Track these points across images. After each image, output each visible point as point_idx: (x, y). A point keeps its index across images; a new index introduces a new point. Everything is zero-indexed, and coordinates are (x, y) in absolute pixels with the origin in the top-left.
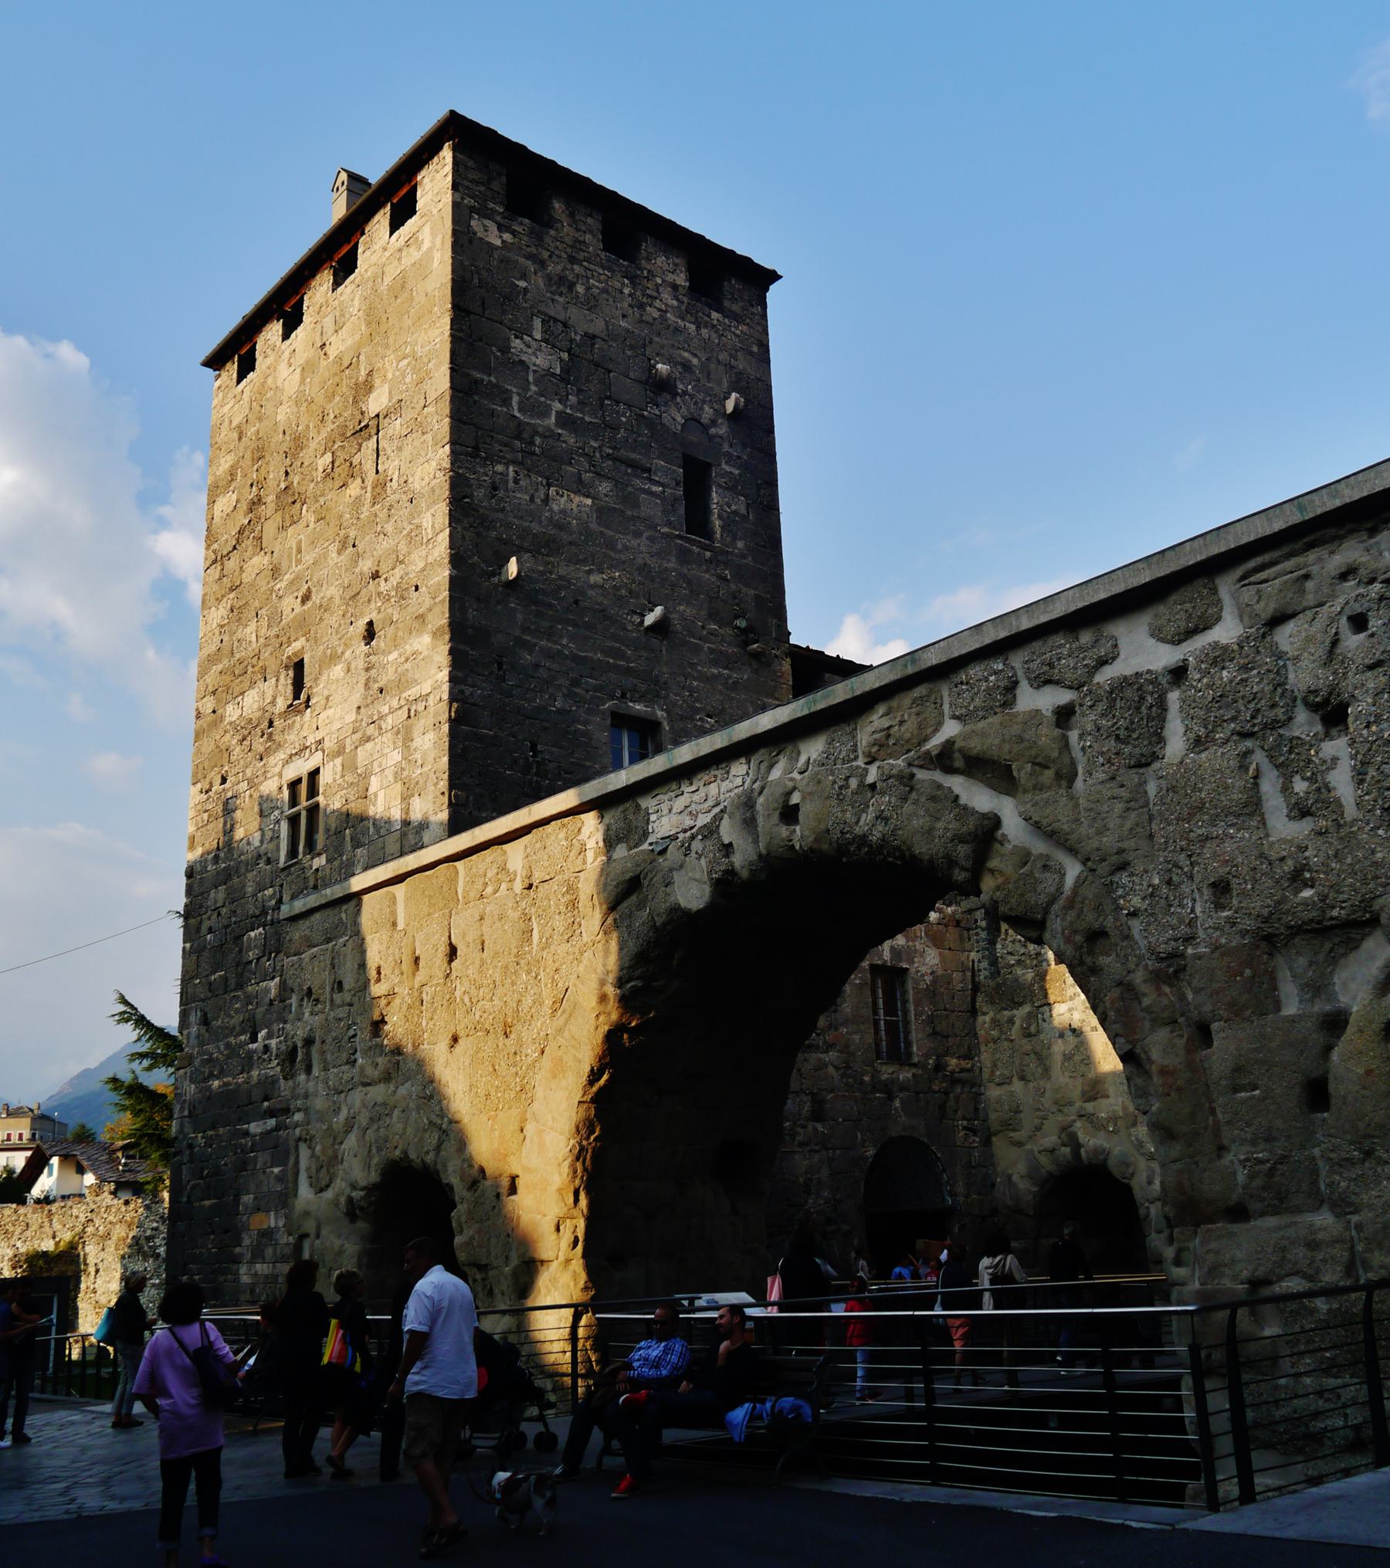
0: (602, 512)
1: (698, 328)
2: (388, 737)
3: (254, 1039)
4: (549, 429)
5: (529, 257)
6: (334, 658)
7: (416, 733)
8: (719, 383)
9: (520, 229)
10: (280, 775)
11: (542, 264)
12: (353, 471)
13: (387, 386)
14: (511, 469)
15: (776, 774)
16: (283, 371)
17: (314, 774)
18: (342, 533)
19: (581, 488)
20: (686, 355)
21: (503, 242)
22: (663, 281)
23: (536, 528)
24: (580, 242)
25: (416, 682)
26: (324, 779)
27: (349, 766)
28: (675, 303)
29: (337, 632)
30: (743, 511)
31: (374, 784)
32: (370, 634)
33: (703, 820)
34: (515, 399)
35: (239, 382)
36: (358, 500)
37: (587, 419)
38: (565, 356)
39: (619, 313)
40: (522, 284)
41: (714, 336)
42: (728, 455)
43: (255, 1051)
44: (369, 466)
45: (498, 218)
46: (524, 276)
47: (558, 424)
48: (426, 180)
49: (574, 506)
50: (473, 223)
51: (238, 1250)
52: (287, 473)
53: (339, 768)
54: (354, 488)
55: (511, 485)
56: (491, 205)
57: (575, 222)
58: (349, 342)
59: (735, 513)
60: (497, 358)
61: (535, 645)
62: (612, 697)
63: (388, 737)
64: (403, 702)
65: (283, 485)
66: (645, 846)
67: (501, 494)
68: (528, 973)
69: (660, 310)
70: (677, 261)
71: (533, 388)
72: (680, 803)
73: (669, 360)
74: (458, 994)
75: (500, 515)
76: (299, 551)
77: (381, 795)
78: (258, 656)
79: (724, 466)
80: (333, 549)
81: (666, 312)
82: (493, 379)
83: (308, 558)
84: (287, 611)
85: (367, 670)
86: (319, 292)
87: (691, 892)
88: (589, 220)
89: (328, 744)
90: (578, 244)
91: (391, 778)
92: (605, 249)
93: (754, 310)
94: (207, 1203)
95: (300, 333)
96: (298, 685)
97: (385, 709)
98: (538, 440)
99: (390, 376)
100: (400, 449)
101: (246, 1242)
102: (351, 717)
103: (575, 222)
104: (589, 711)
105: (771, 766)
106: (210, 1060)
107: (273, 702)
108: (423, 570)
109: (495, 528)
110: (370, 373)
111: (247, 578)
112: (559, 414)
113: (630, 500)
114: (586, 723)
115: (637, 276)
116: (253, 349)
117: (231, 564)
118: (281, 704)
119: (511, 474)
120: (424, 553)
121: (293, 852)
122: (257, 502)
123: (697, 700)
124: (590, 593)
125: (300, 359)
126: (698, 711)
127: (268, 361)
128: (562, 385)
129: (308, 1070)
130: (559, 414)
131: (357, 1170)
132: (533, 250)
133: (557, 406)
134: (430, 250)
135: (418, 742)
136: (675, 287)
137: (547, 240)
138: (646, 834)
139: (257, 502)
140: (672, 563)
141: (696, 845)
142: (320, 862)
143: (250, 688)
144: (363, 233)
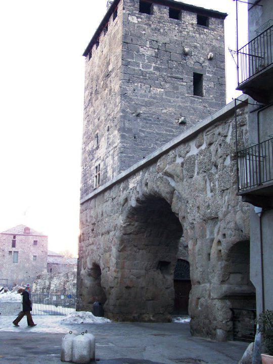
4: (151, 71)
5: (146, 24)
8: (206, 50)
11: (150, 25)
19: (161, 86)
20: (195, 43)
23: (146, 99)
25: (115, 143)
27: (105, 164)
30: (213, 86)
34: (141, 65)
38: (156, 50)
39: (174, 35)
40: (144, 32)
45: (137, 15)
46: (144, 30)
54: (106, 91)
55: (139, 88)
56: (134, 12)
59: (210, 87)
67: (136, 91)
73: (190, 46)
75: (136, 97)
78: (91, 134)
82: (134, 60)
85: (108, 139)
87: (133, 203)
88: (165, 10)
92: (170, 17)
95: (99, 47)
98: (148, 75)
107: (93, 146)
112: (154, 67)
113: (176, 88)
117: (88, 109)
118: (95, 147)
122: (91, 93)
130: (154, 67)
131: (89, 265)
133: (154, 65)
136: (192, 24)
137: (152, 18)
139: (91, 93)
140: (188, 104)
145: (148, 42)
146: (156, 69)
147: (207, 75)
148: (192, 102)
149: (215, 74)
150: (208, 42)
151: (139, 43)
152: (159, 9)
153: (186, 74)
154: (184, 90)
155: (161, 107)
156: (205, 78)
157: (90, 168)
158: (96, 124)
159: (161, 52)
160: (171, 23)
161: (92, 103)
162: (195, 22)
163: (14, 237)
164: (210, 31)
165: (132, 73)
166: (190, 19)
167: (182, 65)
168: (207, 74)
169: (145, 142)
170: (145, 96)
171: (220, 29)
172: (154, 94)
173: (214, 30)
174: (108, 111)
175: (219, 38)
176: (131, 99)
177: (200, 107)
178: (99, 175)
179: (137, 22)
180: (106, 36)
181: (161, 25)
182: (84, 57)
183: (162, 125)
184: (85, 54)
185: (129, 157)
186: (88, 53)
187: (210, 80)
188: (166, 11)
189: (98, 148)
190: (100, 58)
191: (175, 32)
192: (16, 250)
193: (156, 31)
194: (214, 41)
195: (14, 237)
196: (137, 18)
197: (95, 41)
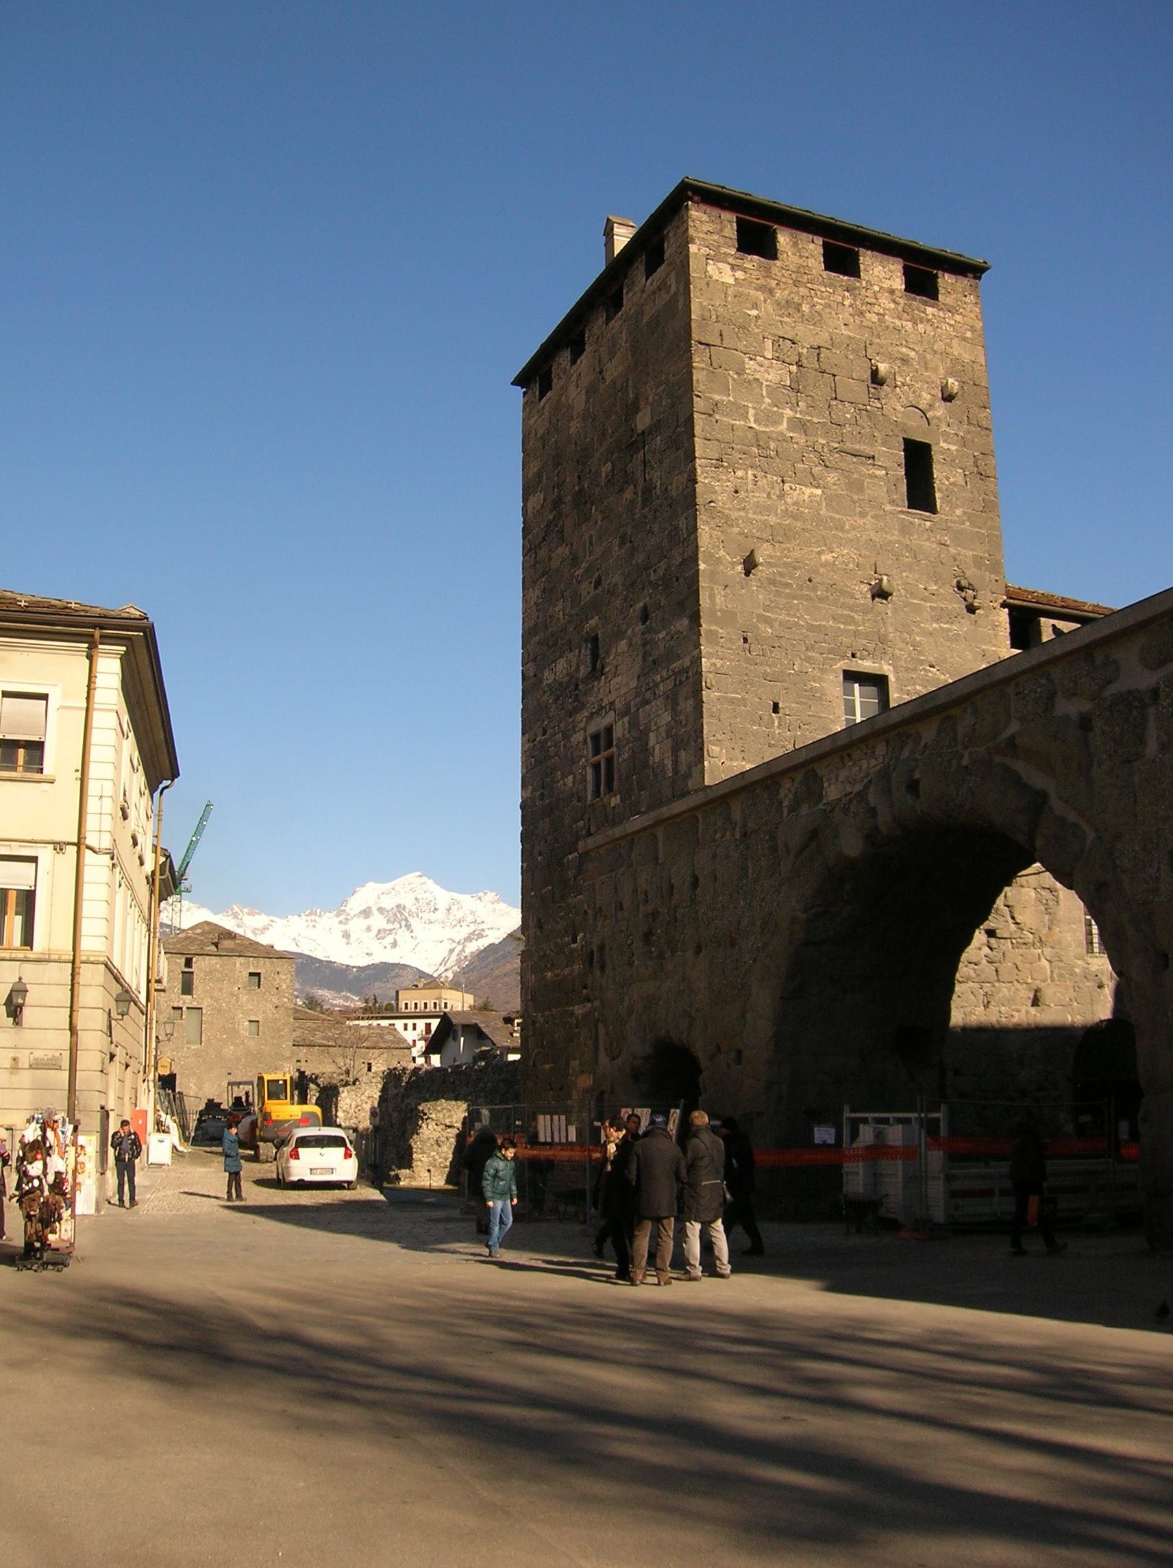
0: (830, 500)
1: (915, 323)
2: (659, 702)
3: (575, 941)
4: (781, 433)
5: (760, 288)
6: (619, 634)
7: (681, 700)
8: (935, 370)
9: (750, 266)
10: (585, 729)
11: (771, 292)
12: (628, 479)
13: (649, 408)
14: (750, 472)
15: (905, 754)
16: (573, 391)
17: (609, 730)
18: (621, 530)
19: (814, 482)
20: (904, 350)
21: (736, 279)
22: (881, 288)
23: (772, 520)
24: (804, 267)
25: (679, 657)
26: (618, 733)
27: (634, 724)
28: (892, 305)
29: (621, 613)
30: (961, 481)
31: (652, 739)
32: (645, 616)
33: (858, 787)
34: (751, 412)
35: (540, 399)
36: (633, 501)
37: (816, 420)
38: (794, 368)
39: (841, 323)
40: (754, 312)
41: (929, 329)
42: (945, 433)
43: (576, 950)
44: (639, 474)
45: (731, 260)
46: (755, 306)
47: (789, 429)
48: (671, 235)
49: (806, 497)
50: (709, 268)
51: (569, 1102)
52: (579, 477)
53: (627, 726)
54: (628, 495)
55: (750, 486)
56: (724, 250)
57: (799, 250)
58: (620, 369)
59: (954, 484)
60: (734, 380)
61: (775, 620)
62: (843, 657)
63: (659, 702)
64: (670, 673)
65: (577, 488)
66: (821, 806)
67: (742, 494)
68: (745, 900)
69: (878, 314)
70: (892, 267)
71: (768, 400)
72: (843, 775)
73: (890, 358)
74: (700, 915)
75: (742, 514)
76: (591, 543)
77: (657, 748)
78: (564, 630)
79: (942, 444)
80: (617, 542)
81: (883, 315)
82: (731, 399)
83: (598, 551)
84: (584, 593)
85: (644, 645)
86: (597, 327)
87: (851, 844)
88: (812, 246)
89: (618, 705)
90: (801, 270)
91: (664, 735)
92: (826, 269)
93: (967, 300)
94: (547, 1066)
95: (584, 360)
96: (595, 655)
97: (658, 678)
98: (772, 445)
99: (651, 399)
100: (661, 462)
101: (575, 1096)
102: (633, 684)
103: (799, 250)
104: (822, 671)
105: (902, 748)
106: (544, 956)
107: (578, 668)
108: (681, 564)
109: (738, 526)
110: (636, 398)
111: (555, 564)
112: (790, 420)
113: (856, 486)
114: (820, 680)
115: (855, 288)
116: (550, 372)
117: (542, 553)
118: (583, 671)
119: (750, 476)
120: (681, 550)
121: (597, 792)
122: (557, 503)
123: (920, 653)
124: (822, 570)
125: (585, 382)
126: (922, 662)
127: (562, 382)
128: (792, 394)
129: (602, 968)
130: (790, 420)
132: (762, 281)
133: (788, 412)
134: (676, 294)
135: (682, 706)
136: (892, 292)
137: (775, 270)
138: (821, 797)
139: (557, 503)
140: (895, 536)
141: (853, 808)
142: (615, 800)
143: (561, 657)
144: (626, 277)
145: (769, 343)
146: (800, 425)
147: (943, 449)
148: (905, 529)
149: (964, 443)
150: (939, 346)
151: (741, 346)
152: (795, 244)
153: (884, 444)
154: (880, 492)
155: (817, 544)
156: (937, 457)
157: (567, 737)
158: (585, 599)
159: (809, 371)
160: (831, 285)
161: (561, 532)
162: (899, 283)
163: (189, 963)
164: (941, 314)
165: (728, 436)
166: (883, 275)
167: (870, 415)
168: (942, 444)
169: (777, 653)
170: (769, 509)
171: (969, 307)
172: (794, 504)
173: (952, 310)
174: (640, 558)
175: (969, 334)
176: (728, 517)
177: (930, 546)
178: (609, 760)
179: (732, 281)
180: (616, 324)
181: (803, 291)
182: (519, 391)
183: (821, 599)
184: (521, 381)
185: (732, 701)
186: (535, 377)
187: (950, 461)
188: (814, 247)
189: (597, 670)
190: (591, 390)
191: (845, 315)
192: (195, 1004)
193: (790, 311)
194: (955, 342)
195: (189, 963)
196: (733, 267)
197: (569, 336)
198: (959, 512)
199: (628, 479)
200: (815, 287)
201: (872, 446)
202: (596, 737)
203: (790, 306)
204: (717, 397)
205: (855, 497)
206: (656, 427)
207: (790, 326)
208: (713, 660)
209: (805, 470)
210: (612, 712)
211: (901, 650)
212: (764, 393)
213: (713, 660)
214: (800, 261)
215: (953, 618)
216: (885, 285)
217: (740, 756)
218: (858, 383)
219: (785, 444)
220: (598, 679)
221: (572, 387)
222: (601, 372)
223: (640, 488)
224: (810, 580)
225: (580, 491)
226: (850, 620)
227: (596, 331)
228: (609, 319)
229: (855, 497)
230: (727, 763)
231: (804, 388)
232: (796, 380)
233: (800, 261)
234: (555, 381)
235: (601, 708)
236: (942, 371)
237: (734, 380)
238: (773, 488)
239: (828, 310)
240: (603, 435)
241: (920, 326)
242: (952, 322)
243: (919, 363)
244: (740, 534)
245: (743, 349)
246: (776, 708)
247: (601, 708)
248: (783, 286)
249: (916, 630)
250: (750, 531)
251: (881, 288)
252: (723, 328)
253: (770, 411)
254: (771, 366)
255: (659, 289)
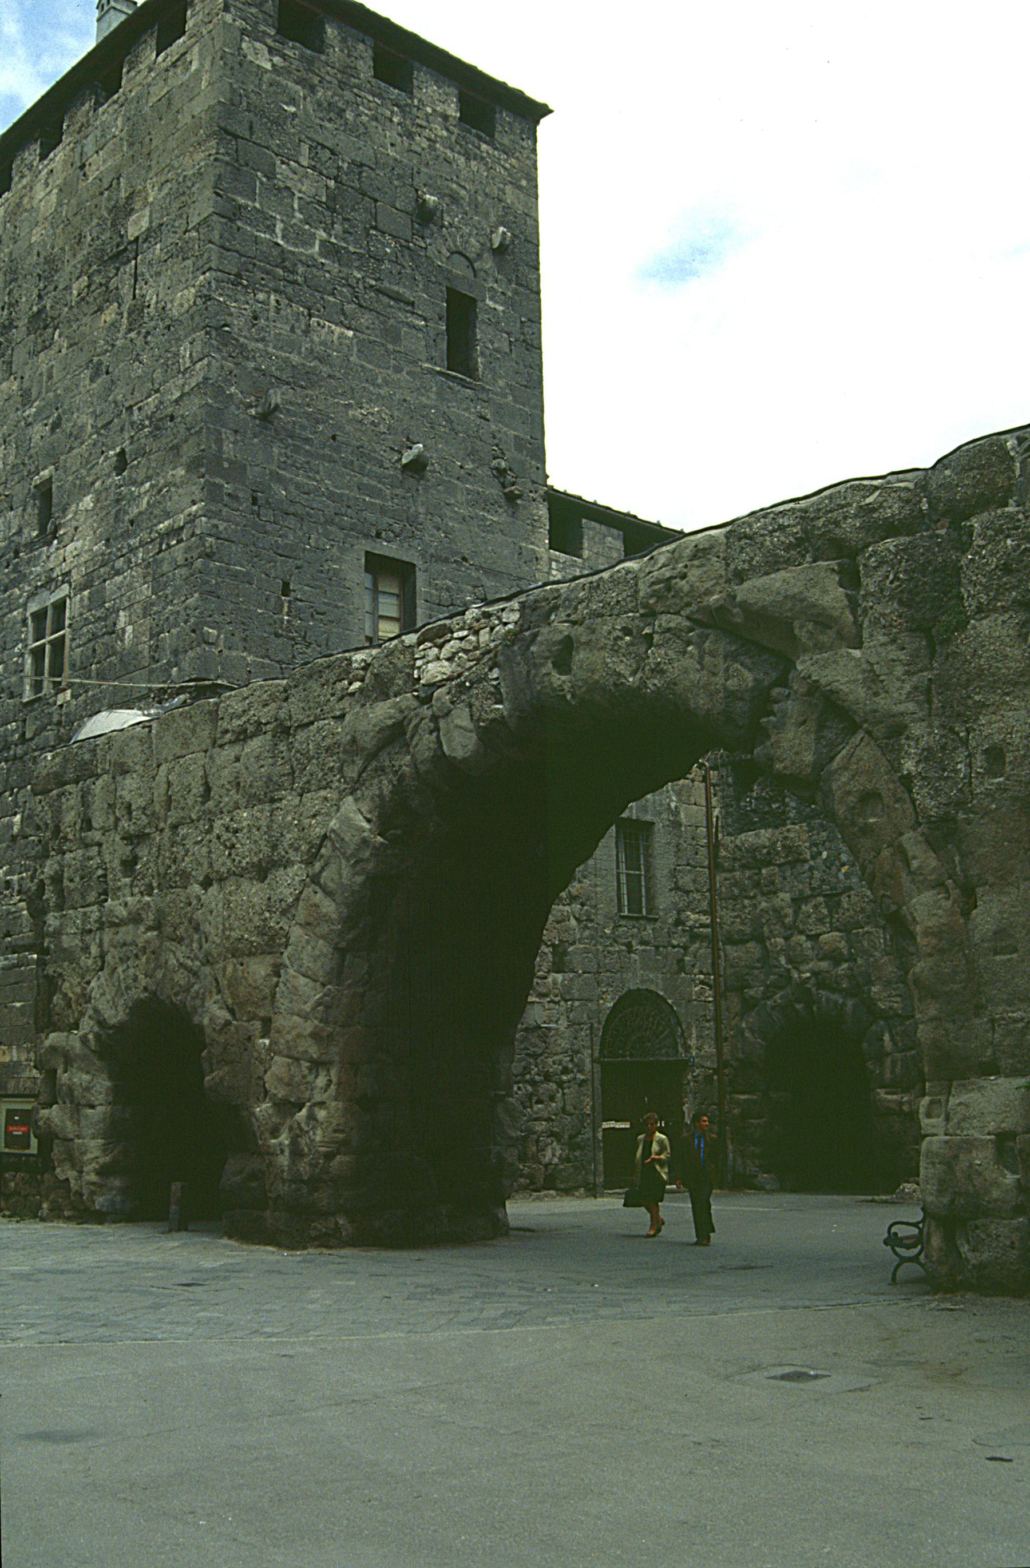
0: (364, 346)
1: (468, 159)
4: (312, 257)
6: (84, 488)
8: (487, 216)
11: (312, 89)
12: (110, 295)
13: (147, 212)
14: (272, 297)
16: (40, 192)
17: (60, 606)
21: (273, 65)
22: (434, 110)
23: (295, 358)
27: (97, 600)
28: (445, 133)
32: (122, 463)
34: (279, 226)
36: (114, 326)
38: (332, 183)
39: (388, 141)
40: (292, 109)
44: (126, 290)
46: (292, 101)
47: (321, 254)
50: (244, 45)
53: (86, 602)
54: (109, 315)
55: (272, 314)
56: (262, 28)
59: (496, 350)
60: (262, 183)
69: (429, 140)
75: (260, 345)
79: (488, 302)
81: (435, 142)
82: (257, 205)
89: (75, 576)
93: (524, 144)
95: (59, 155)
98: (301, 269)
110: (130, 197)
114: (339, 560)
119: (273, 303)
120: (181, 382)
124: (348, 428)
132: (303, 74)
136: (446, 117)
145: (305, 148)
152: (344, 40)
160: (380, 96)
164: (496, 153)
166: (438, 100)
170: (293, 346)
172: (321, 343)
174: (119, 394)
178: (58, 645)
179: (268, 66)
185: (235, 575)
188: (614, 543)
189: (49, 532)
193: (332, 115)
196: (271, 51)
198: (501, 383)
199: (110, 295)
200: (363, 94)
201: (411, 289)
202: (39, 616)
203: (334, 111)
204: (242, 201)
205: (390, 346)
206: (151, 234)
207: (330, 133)
208: (215, 522)
209: (335, 304)
210: (66, 586)
211: (432, 536)
212: (296, 206)
213: (215, 522)
214: (348, 61)
215: (488, 504)
216: (438, 109)
217: (241, 645)
218: (403, 215)
219: (314, 270)
220: (49, 544)
221: (39, 187)
222: (82, 167)
223: (125, 308)
224: (334, 438)
225: (39, 312)
226: (374, 493)
227: (80, 117)
228: (98, 104)
229: (390, 346)
230: (226, 652)
231: (341, 207)
232: (332, 197)
233: (348, 61)
234: (16, 179)
235: (50, 580)
236: (493, 219)
237: (262, 183)
238: (298, 320)
239: (374, 123)
240: (79, 242)
241: (473, 163)
242: (507, 166)
243: (469, 205)
244: (256, 369)
245: (276, 149)
246: (286, 590)
247: (50, 580)
248: (326, 85)
249: (448, 513)
250: (268, 367)
251: (434, 110)
252: (255, 119)
253: (301, 229)
254: (306, 176)
255: (174, 65)
